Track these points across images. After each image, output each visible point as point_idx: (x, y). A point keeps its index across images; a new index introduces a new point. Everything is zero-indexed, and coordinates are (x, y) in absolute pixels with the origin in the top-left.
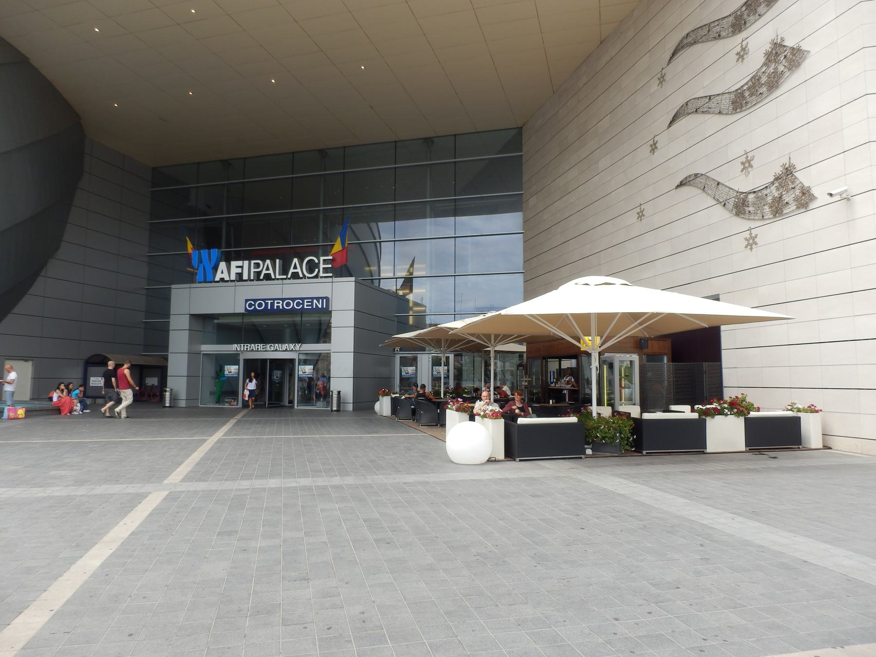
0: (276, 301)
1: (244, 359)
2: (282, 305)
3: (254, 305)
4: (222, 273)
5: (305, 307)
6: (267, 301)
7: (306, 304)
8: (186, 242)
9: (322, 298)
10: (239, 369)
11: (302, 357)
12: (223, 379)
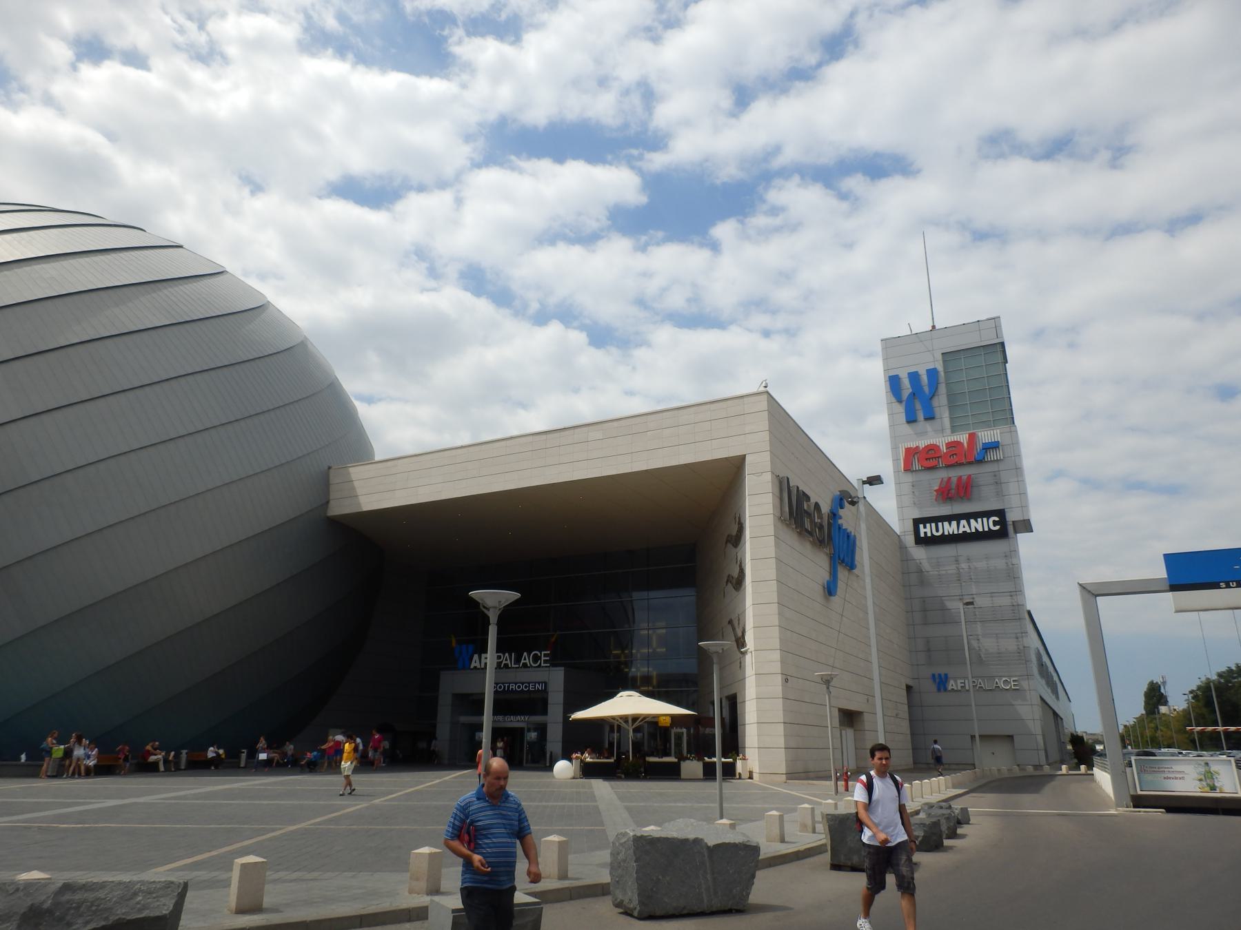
9: (542, 683)
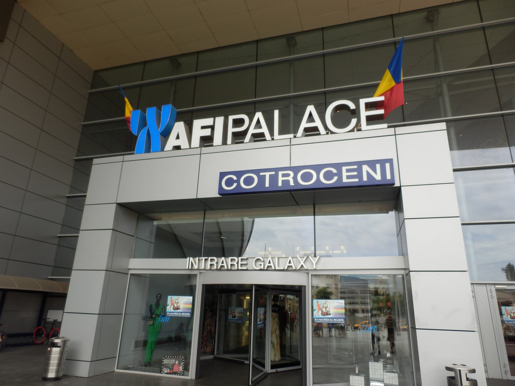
0: (280, 173)
1: (203, 285)
2: (295, 178)
3: (238, 181)
4: (178, 137)
5: (345, 180)
6: (261, 174)
7: (345, 174)
8: (124, 103)
9: (382, 162)
10: (193, 304)
11: (322, 284)
12: (163, 320)
